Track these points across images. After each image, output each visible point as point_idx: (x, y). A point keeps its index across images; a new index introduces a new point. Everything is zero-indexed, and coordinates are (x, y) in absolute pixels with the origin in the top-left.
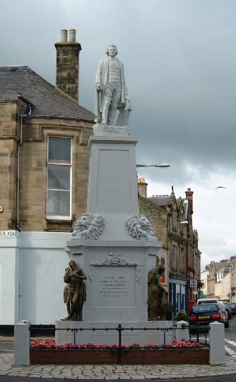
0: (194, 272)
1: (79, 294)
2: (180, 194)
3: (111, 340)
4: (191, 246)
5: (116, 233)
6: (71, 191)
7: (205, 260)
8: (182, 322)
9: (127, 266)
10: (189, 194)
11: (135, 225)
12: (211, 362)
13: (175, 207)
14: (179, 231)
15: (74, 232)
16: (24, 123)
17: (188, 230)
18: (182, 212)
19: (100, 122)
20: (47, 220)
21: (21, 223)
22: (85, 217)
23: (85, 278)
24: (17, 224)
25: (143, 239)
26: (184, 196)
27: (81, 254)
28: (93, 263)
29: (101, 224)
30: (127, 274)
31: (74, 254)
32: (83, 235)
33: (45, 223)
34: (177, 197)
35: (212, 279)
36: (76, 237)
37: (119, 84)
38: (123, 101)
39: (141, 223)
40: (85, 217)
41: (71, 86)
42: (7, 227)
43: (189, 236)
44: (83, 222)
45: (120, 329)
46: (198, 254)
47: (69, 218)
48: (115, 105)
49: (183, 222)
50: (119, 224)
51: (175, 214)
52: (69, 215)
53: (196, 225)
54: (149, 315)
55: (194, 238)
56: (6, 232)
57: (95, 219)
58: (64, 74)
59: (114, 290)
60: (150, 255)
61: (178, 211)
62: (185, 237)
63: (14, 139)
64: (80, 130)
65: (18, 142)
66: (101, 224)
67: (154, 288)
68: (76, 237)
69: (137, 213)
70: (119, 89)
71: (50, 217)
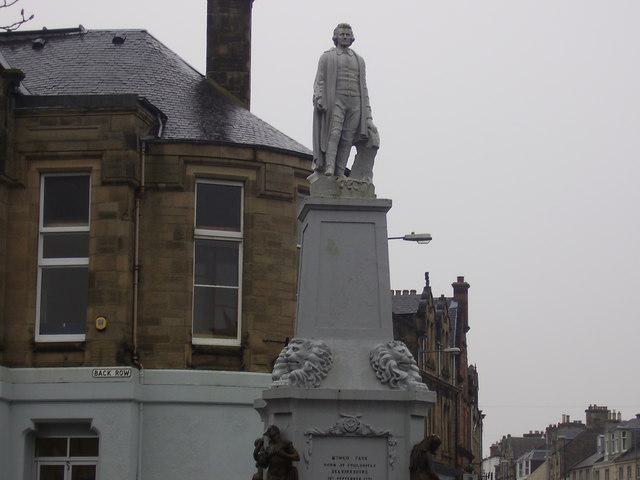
0: (470, 457)
2: (443, 289)
4: (465, 401)
5: (354, 379)
6: (240, 288)
7: (492, 434)
9: (372, 436)
10: (461, 288)
11: (387, 360)
13: (431, 317)
14: (440, 368)
15: (276, 372)
16: (147, 153)
17: (458, 365)
18: (445, 327)
19: (321, 170)
20: (193, 347)
21: (142, 353)
22: (294, 345)
23: (297, 459)
24: (133, 355)
25: (403, 388)
26: (450, 293)
29: (325, 358)
30: (372, 451)
31: (276, 414)
32: (292, 378)
33: (188, 352)
34: (436, 294)
36: (280, 382)
37: (358, 98)
38: (364, 131)
39: (397, 358)
40: (294, 345)
41: (235, 75)
42: (114, 361)
43: (460, 380)
44: (293, 355)
46: (480, 417)
47: (235, 342)
49: (449, 349)
50: (356, 359)
51: (431, 333)
52: (234, 335)
53: (473, 358)
55: (470, 383)
56: (113, 371)
57: (315, 350)
58: (223, 50)
60: (413, 416)
61: (438, 326)
62: (453, 382)
63: (130, 185)
64: (259, 168)
66: (325, 358)
68: (280, 382)
69: (390, 339)
70: (358, 108)
71: (198, 341)
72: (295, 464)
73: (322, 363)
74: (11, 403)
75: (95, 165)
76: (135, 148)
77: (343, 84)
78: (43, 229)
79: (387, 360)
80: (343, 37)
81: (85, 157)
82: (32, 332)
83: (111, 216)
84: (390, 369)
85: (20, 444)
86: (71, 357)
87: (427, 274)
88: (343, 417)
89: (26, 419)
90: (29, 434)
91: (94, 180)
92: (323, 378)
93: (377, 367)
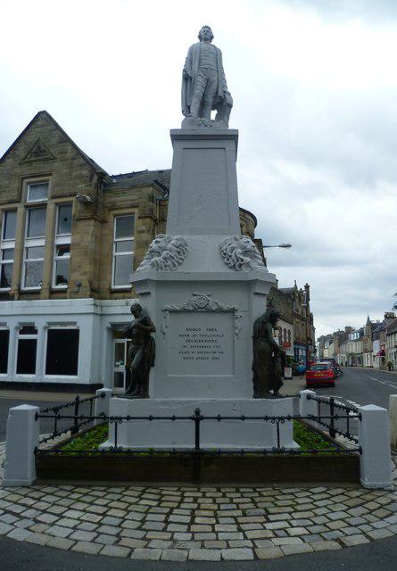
1: (144, 355)
2: (301, 286)
3: (179, 440)
7: (317, 336)
8: (308, 391)
9: (221, 311)
10: (307, 287)
11: (233, 249)
12: (366, 482)
26: (303, 289)
27: (149, 293)
28: (169, 307)
29: (181, 249)
30: (222, 323)
32: (153, 265)
35: (322, 347)
38: (220, 94)
39: (243, 248)
45: (198, 418)
46: (314, 329)
48: (210, 100)
51: (297, 300)
54: (255, 388)
57: (172, 242)
59: (200, 350)
65: (156, 221)
66: (181, 249)
67: (263, 344)
70: (216, 78)
72: (153, 335)
73: (179, 253)
74: (101, 315)
75: (136, 210)
76: (153, 202)
77: (204, 62)
78: (115, 240)
79: (233, 249)
80: (206, 35)
81: (132, 207)
82: (110, 284)
83: (142, 232)
84: (236, 256)
85: (105, 333)
86: (126, 294)
87: (289, 246)
88: (195, 295)
89: (108, 322)
90: (109, 329)
91: (136, 216)
92: (179, 264)
93: (225, 254)
